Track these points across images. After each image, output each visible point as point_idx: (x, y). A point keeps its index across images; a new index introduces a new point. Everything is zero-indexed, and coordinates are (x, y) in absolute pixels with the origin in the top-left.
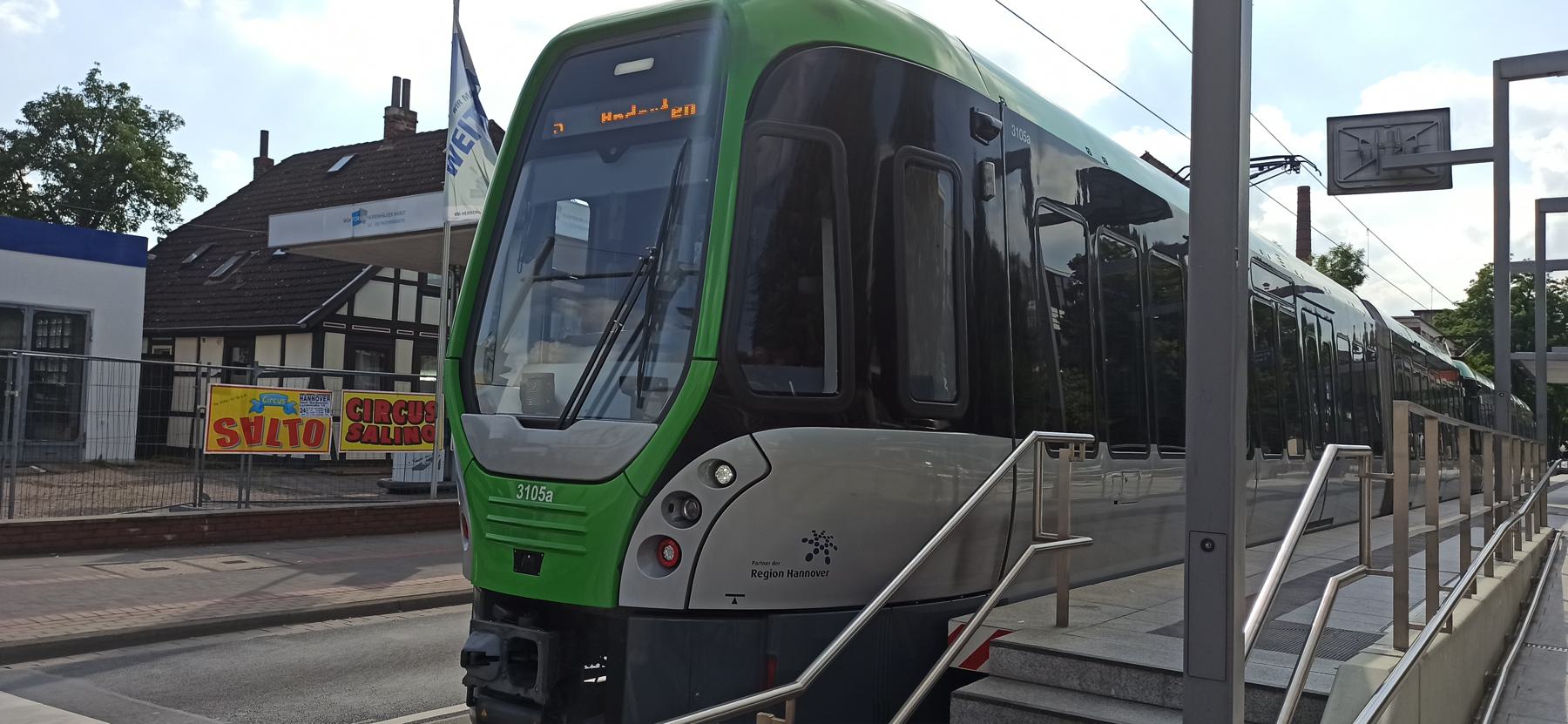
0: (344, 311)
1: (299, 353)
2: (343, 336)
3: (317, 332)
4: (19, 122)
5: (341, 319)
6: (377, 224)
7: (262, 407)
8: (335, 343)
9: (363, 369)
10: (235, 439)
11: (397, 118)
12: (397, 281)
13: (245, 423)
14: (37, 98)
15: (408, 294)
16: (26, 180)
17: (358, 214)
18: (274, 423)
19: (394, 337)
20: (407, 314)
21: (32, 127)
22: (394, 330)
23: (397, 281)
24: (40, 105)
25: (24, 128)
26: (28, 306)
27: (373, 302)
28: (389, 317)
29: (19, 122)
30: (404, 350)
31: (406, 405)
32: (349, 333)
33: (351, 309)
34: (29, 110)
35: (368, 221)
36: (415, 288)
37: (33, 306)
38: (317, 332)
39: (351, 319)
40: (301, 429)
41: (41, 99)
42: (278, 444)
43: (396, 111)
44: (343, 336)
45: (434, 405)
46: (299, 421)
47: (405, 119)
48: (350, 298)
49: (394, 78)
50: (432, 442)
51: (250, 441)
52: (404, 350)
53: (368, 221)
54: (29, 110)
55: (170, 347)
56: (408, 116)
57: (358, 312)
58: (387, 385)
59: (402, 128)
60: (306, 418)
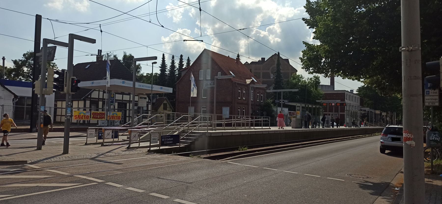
0: (89, 97)
1: (81, 104)
2: (102, 102)
3: (85, 100)
4: (23, 58)
5: (89, 98)
6: (128, 84)
7: (80, 114)
8: (88, 102)
9: (93, 107)
10: (111, 118)
11: (99, 58)
12: (99, 91)
13: (79, 116)
14: (26, 53)
15: (101, 93)
16: (24, 69)
17: (161, 88)
18: (82, 116)
19: (98, 101)
20: (101, 97)
21: (25, 59)
22: (130, 102)
23: (99, 91)
24: (26, 54)
25: (24, 59)
26: (26, 97)
27: (95, 95)
28: (98, 97)
29: (23, 58)
30: (100, 103)
31: (101, 113)
32: (91, 101)
33: (91, 96)
34: (24, 55)
35: (125, 84)
36: (103, 92)
37: (27, 97)
38: (85, 100)
39: (91, 98)
40: (86, 117)
41: (26, 53)
42: (83, 119)
43: (99, 56)
44: (102, 102)
45: (105, 113)
46: (85, 116)
47: (101, 58)
48: (90, 94)
49: (98, 50)
50: (104, 118)
51: (112, 119)
52: (100, 103)
53: (125, 84)
54: (24, 55)
55: (56, 103)
56: (101, 57)
57: (92, 97)
58: (98, 110)
59: (100, 59)
60: (86, 115)
